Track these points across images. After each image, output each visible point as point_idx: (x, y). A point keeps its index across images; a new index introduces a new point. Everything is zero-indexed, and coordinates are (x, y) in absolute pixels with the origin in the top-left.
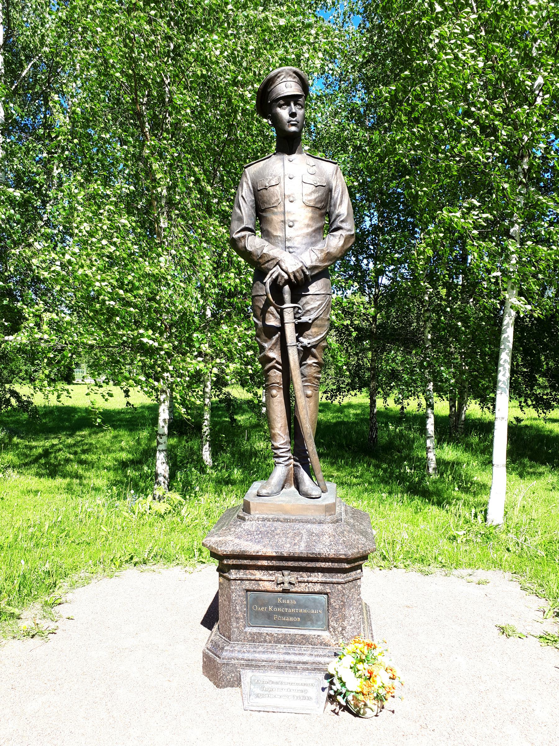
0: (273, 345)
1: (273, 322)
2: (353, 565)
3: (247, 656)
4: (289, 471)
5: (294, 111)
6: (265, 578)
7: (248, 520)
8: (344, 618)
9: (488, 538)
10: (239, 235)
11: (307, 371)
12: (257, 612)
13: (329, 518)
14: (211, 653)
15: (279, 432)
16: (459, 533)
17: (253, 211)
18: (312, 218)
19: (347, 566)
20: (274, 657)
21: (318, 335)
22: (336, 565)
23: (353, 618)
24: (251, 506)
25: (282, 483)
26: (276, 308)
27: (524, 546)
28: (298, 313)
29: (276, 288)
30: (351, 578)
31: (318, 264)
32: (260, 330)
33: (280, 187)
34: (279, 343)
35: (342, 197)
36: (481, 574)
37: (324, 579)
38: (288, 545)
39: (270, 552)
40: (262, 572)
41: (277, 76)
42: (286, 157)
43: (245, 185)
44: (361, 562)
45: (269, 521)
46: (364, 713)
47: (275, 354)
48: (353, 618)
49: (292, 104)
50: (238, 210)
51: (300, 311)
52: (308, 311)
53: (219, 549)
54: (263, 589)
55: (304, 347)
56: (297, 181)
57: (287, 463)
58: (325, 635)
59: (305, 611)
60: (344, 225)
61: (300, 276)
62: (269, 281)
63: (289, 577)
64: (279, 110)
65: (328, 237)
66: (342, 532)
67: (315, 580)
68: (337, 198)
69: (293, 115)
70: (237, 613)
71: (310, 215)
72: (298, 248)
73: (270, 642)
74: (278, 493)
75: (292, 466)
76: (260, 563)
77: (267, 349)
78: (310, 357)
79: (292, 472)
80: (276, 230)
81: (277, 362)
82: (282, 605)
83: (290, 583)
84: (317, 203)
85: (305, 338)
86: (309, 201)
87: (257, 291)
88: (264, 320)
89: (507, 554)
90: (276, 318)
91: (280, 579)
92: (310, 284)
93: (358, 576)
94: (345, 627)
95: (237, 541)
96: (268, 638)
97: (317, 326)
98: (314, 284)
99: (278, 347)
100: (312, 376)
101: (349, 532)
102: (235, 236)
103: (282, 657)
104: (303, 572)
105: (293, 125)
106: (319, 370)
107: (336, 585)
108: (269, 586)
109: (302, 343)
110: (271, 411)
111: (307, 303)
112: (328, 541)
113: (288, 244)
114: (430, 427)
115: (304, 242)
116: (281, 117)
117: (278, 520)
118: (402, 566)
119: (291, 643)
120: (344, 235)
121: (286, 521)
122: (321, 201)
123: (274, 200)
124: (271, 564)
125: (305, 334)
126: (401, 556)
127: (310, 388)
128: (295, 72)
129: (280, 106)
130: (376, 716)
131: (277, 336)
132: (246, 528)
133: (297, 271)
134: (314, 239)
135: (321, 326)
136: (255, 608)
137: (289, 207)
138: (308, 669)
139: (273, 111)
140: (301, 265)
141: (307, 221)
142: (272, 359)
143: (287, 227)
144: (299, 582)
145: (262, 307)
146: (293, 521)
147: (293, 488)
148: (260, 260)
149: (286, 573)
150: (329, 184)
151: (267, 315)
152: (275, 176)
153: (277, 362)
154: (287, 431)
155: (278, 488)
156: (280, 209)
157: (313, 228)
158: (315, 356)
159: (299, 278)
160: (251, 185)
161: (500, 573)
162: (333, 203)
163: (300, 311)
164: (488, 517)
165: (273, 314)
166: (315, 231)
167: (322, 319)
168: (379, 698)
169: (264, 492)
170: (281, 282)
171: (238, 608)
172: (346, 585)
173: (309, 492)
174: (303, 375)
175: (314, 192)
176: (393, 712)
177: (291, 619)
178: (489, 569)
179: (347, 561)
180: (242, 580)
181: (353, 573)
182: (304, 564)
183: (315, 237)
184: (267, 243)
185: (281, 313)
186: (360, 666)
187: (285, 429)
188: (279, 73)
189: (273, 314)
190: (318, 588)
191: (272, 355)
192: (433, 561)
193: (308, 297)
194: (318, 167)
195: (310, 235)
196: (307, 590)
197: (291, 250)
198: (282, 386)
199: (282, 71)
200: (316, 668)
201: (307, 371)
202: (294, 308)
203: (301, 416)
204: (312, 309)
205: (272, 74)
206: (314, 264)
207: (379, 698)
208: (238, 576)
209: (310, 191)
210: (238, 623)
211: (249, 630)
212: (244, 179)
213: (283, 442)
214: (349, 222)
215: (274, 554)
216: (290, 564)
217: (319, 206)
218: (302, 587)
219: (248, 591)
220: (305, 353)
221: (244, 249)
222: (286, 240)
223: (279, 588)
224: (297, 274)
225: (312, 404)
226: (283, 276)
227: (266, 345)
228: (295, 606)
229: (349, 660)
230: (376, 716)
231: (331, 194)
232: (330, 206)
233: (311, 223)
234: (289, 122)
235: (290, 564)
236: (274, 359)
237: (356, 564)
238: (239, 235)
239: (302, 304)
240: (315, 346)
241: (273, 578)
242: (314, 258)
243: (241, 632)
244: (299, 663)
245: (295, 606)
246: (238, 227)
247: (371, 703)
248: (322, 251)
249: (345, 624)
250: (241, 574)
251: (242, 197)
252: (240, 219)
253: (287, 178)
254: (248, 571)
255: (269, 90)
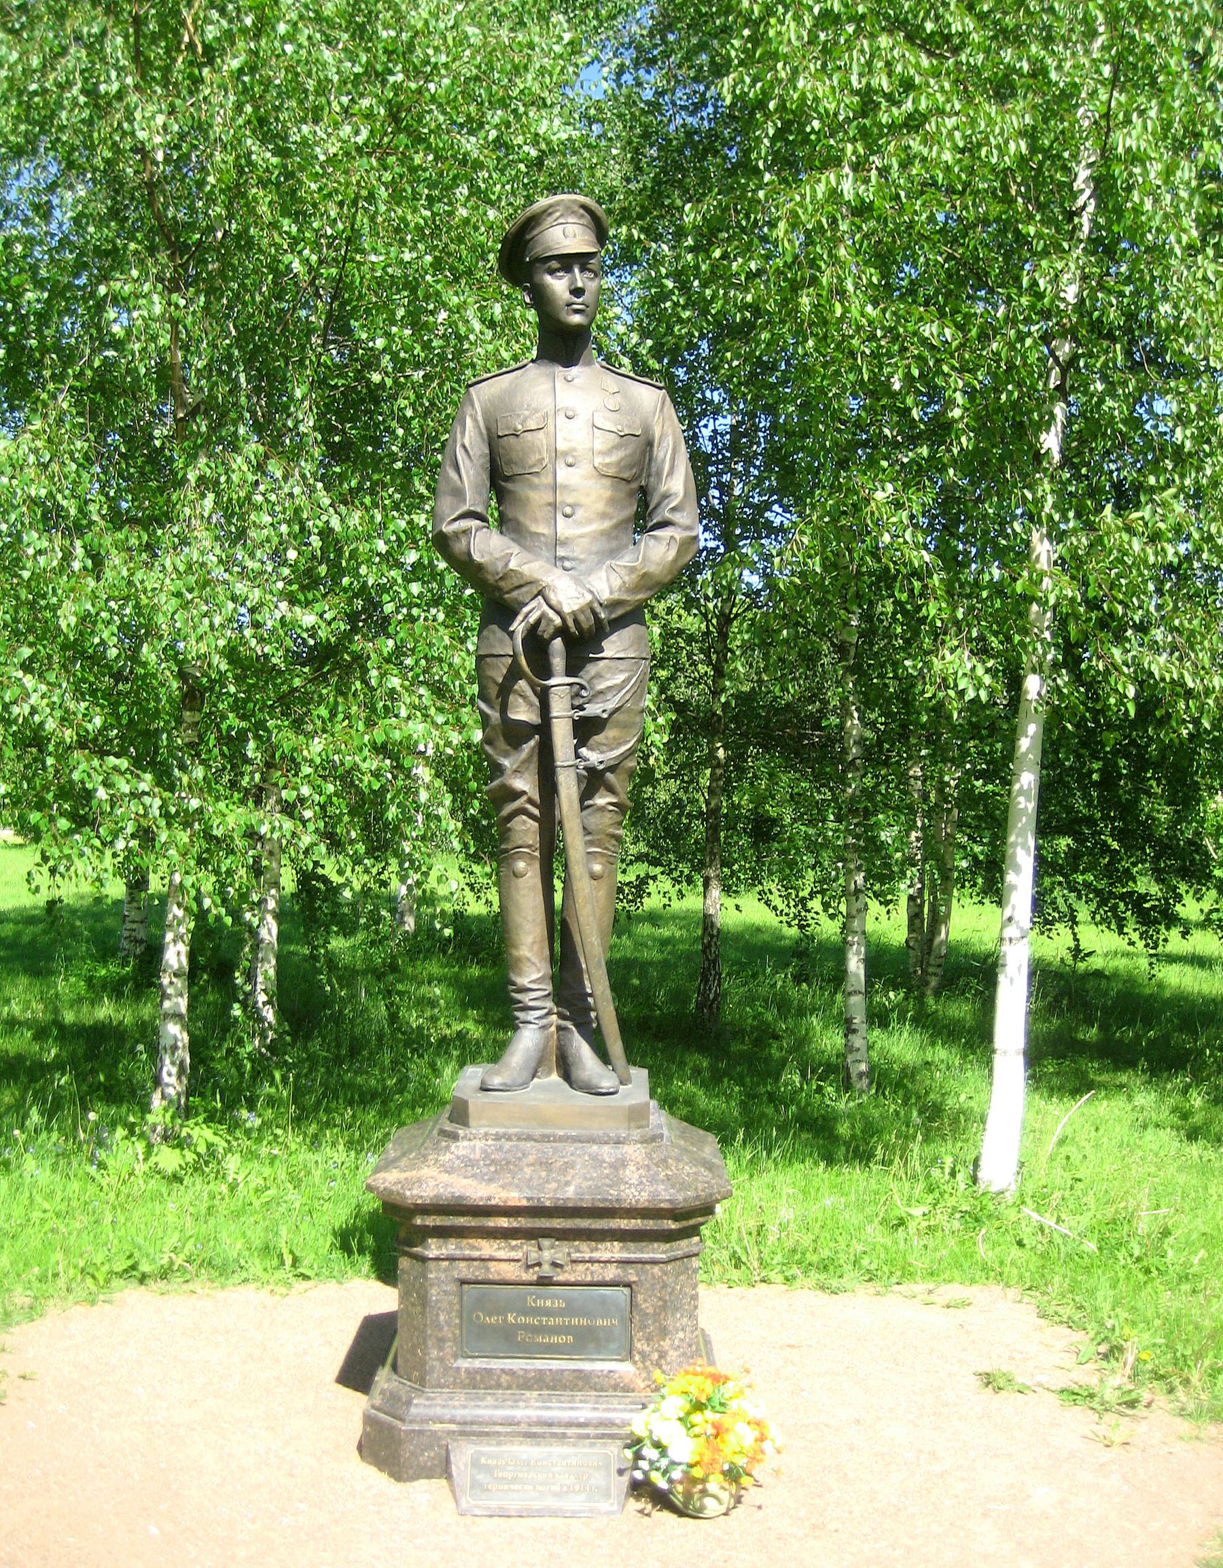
0: (524, 762)
1: (523, 712)
2: (685, 1223)
3: (460, 1413)
4: (548, 1039)
5: (580, 284)
6: (501, 1254)
7: (464, 1138)
8: (664, 1332)
9: (977, 1220)
10: (456, 526)
11: (595, 821)
12: (484, 1327)
13: (636, 1134)
14: (382, 1415)
15: (529, 955)
16: (912, 1211)
17: (485, 477)
18: (612, 501)
19: (672, 1225)
20: (518, 1414)
21: (620, 745)
22: (650, 1224)
23: (681, 1335)
24: (472, 1109)
25: (533, 1064)
26: (533, 686)
27: (1056, 1235)
28: (578, 695)
29: (536, 643)
30: (679, 1253)
31: (625, 597)
32: (494, 728)
33: (547, 434)
34: (535, 759)
35: (673, 459)
36: (954, 1291)
37: (625, 1255)
38: (554, 1185)
39: (515, 1197)
40: (496, 1244)
41: (546, 212)
42: (559, 370)
43: (469, 422)
44: (700, 1219)
45: (509, 1139)
46: (702, 1509)
47: (525, 784)
48: (681, 1335)
49: (576, 270)
50: (453, 474)
51: (584, 693)
52: (601, 692)
53: (408, 1193)
54: (497, 1277)
55: (591, 770)
56: (580, 424)
57: (544, 1021)
58: (625, 1369)
59: (584, 1322)
60: (677, 517)
61: (587, 622)
62: (521, 628)
63: (551, 1251)
64: (548, 279)
65: (645, 540)
66: (664, 1161)
67: (606, 1256)
68: (663, 461)
69: (577, 292)
70: (441, 1329)
71: (608, 493)
72: (582, 561)
73: (509, 1388)
74: (525, 1084)
75: (553, 1029)
76: (492, 1222)
77: (509, 772)
78: (602, 791)
79: (553, 1043)
80: (536, 521)
81: (530, 801)
82: (537, 1311)
83: (555, 1265)
84: (622, 469)
85: (592, 749)
86: (607, 465)
87: (491, 646)
88: (504, 709)
89: (1015, 1251)
90: (531, 705)
91: (534, 1256)
92: (607, 636)
93: (695, 1250)
94: (666, 1353)
95: (445, 1177)
96: (504, 1379)
97: (619, 725)
98: (613, 637)
99: (534, 767)
100: (602, 832)
101: (678, 1160)
102: (447, 529)
103: (533, 1414)
104: (581, 1240)
105: (577, 311)
106: (620, 818)
107: (648, 1267)
108: (511, 1271)
109: (586, 760)
110: (512, 909)
111: (599, 676)
112: (636, 1176)
113: (561, 552)
114: (855, 965)
115: (594, 549)
116: (553, 293)
117: (529, 1138)
118: (780, 1278)
119: (554, 1388)
120: (678, 537)
121: (545, 1138)
122: (631, 467)
123: (533, 458)
124: (515, 1224)
125: (591, 741)
126: (778, 1258)
127: (600, 859)
128: (584, 207)
129: (552, 272)
130: (726, 1514)
131: (532, 743)
132: (461, 1152)
133: (582, 610)
134: (614, 544)
135: (625, 726)
136: (478, 1317)
137: (563, 474)
138: (587, 1436)
139: (537, 279)
140: (589, 597)
141: (600, 507)
142: (517, 795)
143: (560, 517)
144: (574, 1262)
145: (500, 680)
146: (561, 1139)
147: (555, 1077)
148: (502, 584)
149: (546, 1242)
150: (647, 430)
151: (511, 698)
152: (536, 411)
153: (530, 801)
154: (547, 952)
155: (526, 1074)
156: (546, 479)
157: (614, 521)
158: (611, 790)
159: (585, 626)
160: (480, 418)
161: (997, 1289)
162: (654, 469)
163: (584, 693)
164: (980, 1175)
165: (524, 697)
166: (616, 527)
167: (629, 710)
168: (733, 1475)
169: (496, 1081)
170: (546, 631)
171: (442, 1318)
172: (669, 1267)
173: (595, 1081)
174: (586, 831)
175: (616, 447)
176: (760, 1507)
177: (555, 1339)
178: (973, 1281)
179: (674, 1214)
180: (451, 1259)
181: (684, 1243)
182: (584, 1223)
183: (616, 538)
184: (515, 549)
185: (544, 697)
186: (696, 1418)
187: (542, 948)
188: (551, 206)
189: (524, 697)
190: (611, 1273)
191: (519, 784)
192: (850, 1267)
193: (602, 663)
194: (625, 397)
195: (606, 534)
196: (589, 1278)
197: (567, 564)
198: (537, 854)
199: (558, 203)
200: (605, 1431)
201: (595, 821)
202: (570, 685)
203: (581, 919)
204: (610, 688)
205: (536, 207)
206: (616, 596)
207: (733, 1475)
208: (444, 1251)
209: (610, 445)
210: (441, 1349)
211: (464, 1364)
212: (469, 410)
213: (535, 976)
214: (688, 509)
215: (524, 1203)
216: (557, 1223)
217: (625, 475)
218: (579, 1273)
219: (463, 1282)
220: (593, 781)
221: (465, 558)
222: (557, 542)
223: (531, 1276)
224: (582, 618)
225: (602, 893)
226: (551, 620)
227: (506, 763)
228: (560, 1313)
229: (675, 1404)
230: (726, 1514)
231: (651, 451)
232: (649, 475)
233: (610, 510)
234: (569, 305)
235: (557, 1223)
236: (524, 793)
237: (692, 1222)
238: (456, 526)
239: (588, 677)
240: (612, 769)
241: (518, 1255)
242: (617, 583)
243: (447, 1369)
244: (570, 1425)
245: (560, 1313)
246: (454, 510)
247: (715, 1484)
248: (632, 570)
249: (665, 1344)
250: (450, 1247)
251: (464, 446)
252: (458, 493)
253: (561, 418)
254: (465, 1241)
255: (528, 237)
